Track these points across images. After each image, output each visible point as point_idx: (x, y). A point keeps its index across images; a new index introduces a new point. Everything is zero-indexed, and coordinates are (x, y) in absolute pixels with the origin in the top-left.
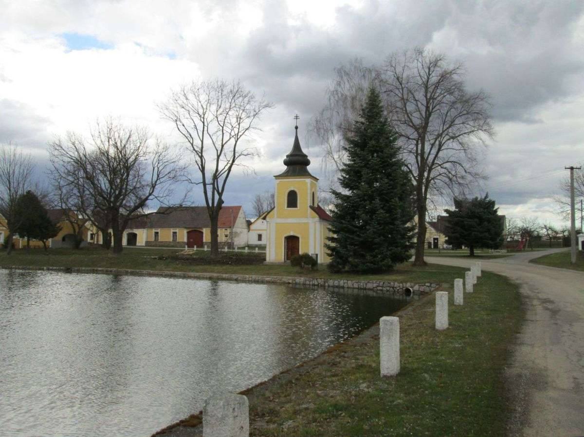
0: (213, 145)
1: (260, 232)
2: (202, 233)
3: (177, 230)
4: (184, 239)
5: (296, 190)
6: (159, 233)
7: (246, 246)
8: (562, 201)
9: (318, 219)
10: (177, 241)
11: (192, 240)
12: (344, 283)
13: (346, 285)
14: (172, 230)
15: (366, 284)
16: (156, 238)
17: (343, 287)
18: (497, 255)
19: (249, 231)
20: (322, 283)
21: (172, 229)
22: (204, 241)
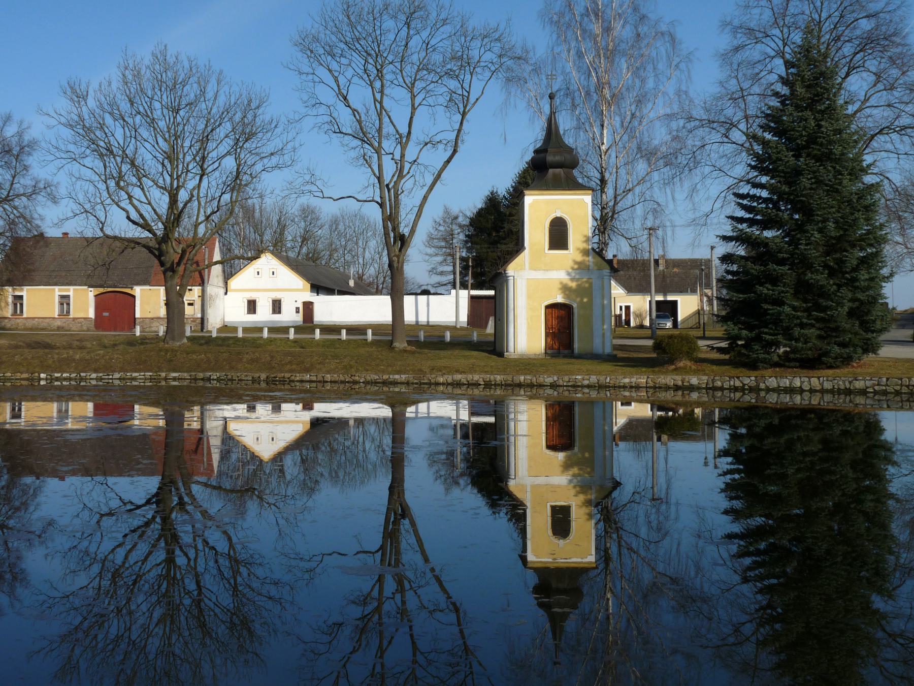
0: (461, 148)
1: (252, 296)
2: (134, 297)
3: (71, 291)
4: (87, 311)
5: (565, 216)
6: (25, 298)
7: (293, 327)
8: (129, 105)
9: (608, 271)
10: (71, 316)
11: (106, 314)
12: (802, 382)
13: (806, 387)
14: (58, 291)
15: (850, 382)
16: (62, 310)
17: (801, 391)
18: (607, 367)
19: (226, 293)
20: (753, 384)
21: (57, 288)
22: (138, 315)
